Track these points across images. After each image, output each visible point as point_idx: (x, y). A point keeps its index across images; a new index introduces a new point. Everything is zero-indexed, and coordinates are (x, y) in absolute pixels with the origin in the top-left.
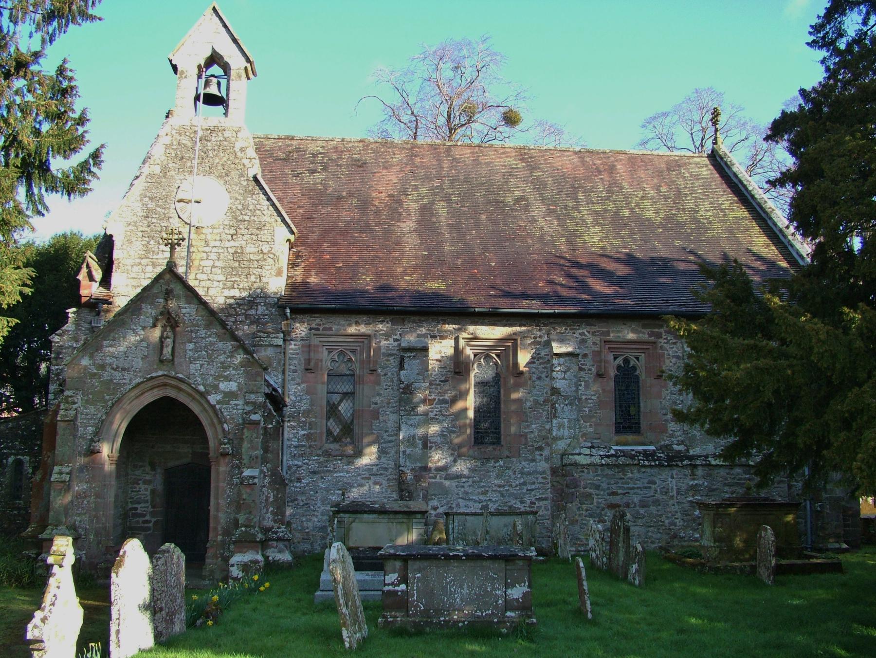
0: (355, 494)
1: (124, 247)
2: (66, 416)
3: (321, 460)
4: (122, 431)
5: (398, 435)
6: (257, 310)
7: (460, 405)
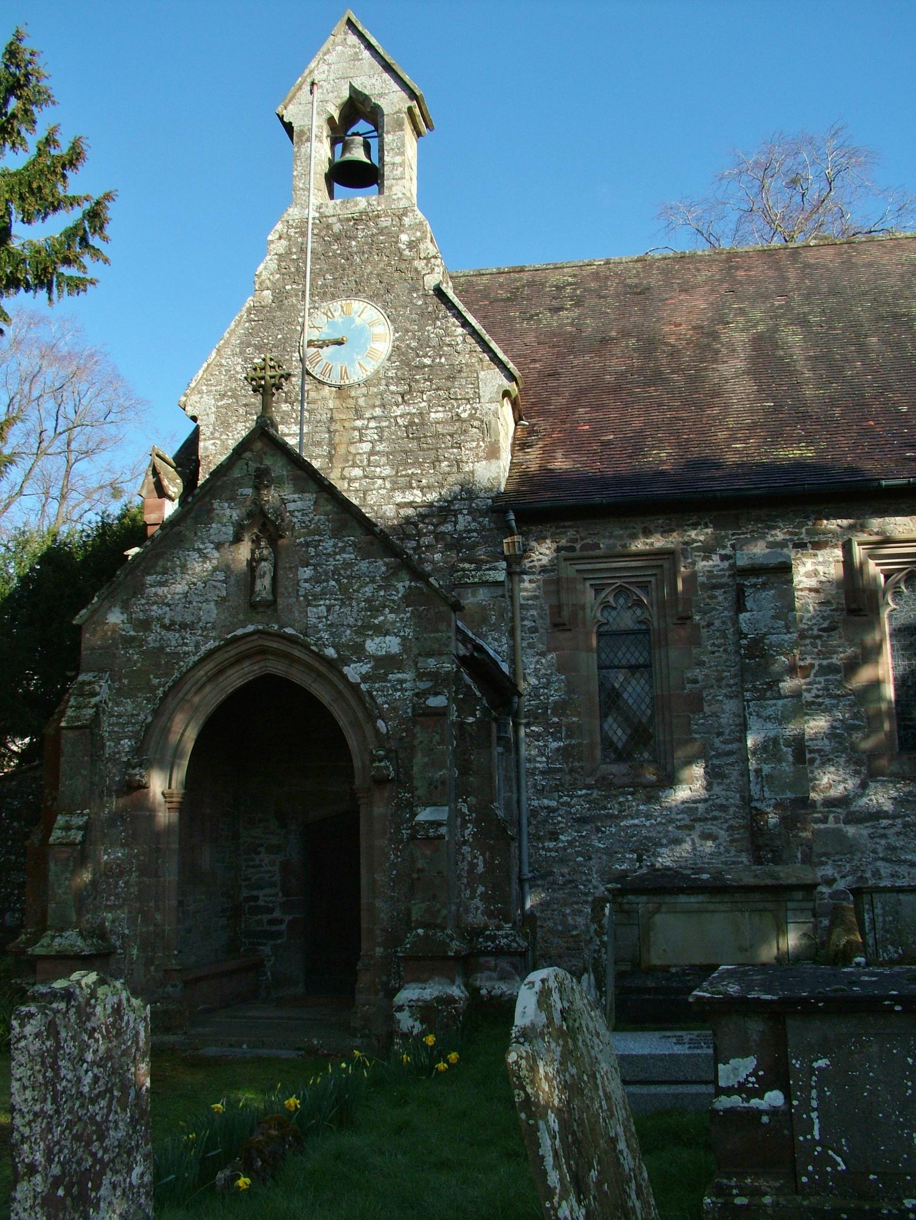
0: (665, 859)
1: (217, 435)
2: (77, 718)
3: (595, 795)
4: (189, 746)
5: (743, 740)
6: (456, 523)
7: (865, 675)
